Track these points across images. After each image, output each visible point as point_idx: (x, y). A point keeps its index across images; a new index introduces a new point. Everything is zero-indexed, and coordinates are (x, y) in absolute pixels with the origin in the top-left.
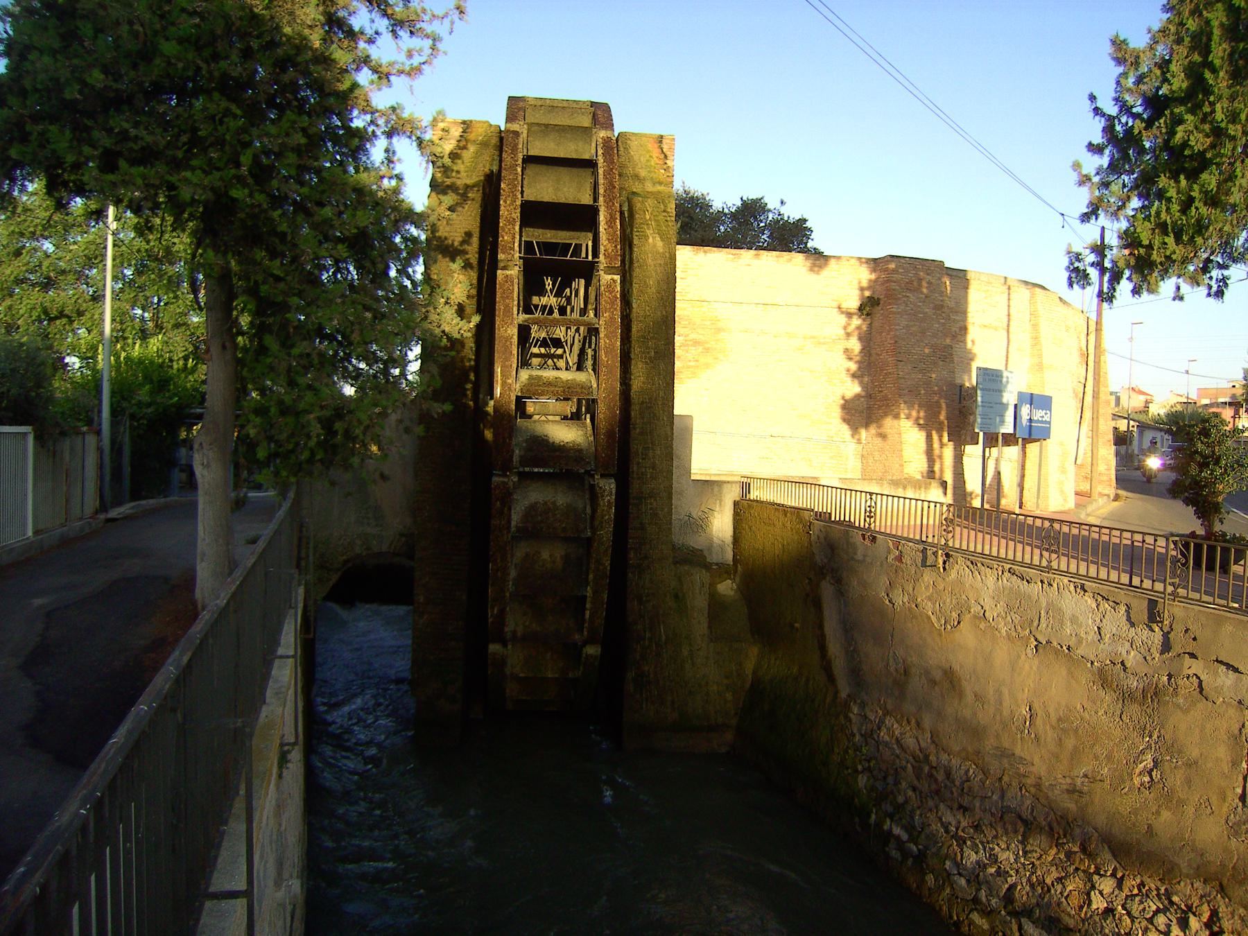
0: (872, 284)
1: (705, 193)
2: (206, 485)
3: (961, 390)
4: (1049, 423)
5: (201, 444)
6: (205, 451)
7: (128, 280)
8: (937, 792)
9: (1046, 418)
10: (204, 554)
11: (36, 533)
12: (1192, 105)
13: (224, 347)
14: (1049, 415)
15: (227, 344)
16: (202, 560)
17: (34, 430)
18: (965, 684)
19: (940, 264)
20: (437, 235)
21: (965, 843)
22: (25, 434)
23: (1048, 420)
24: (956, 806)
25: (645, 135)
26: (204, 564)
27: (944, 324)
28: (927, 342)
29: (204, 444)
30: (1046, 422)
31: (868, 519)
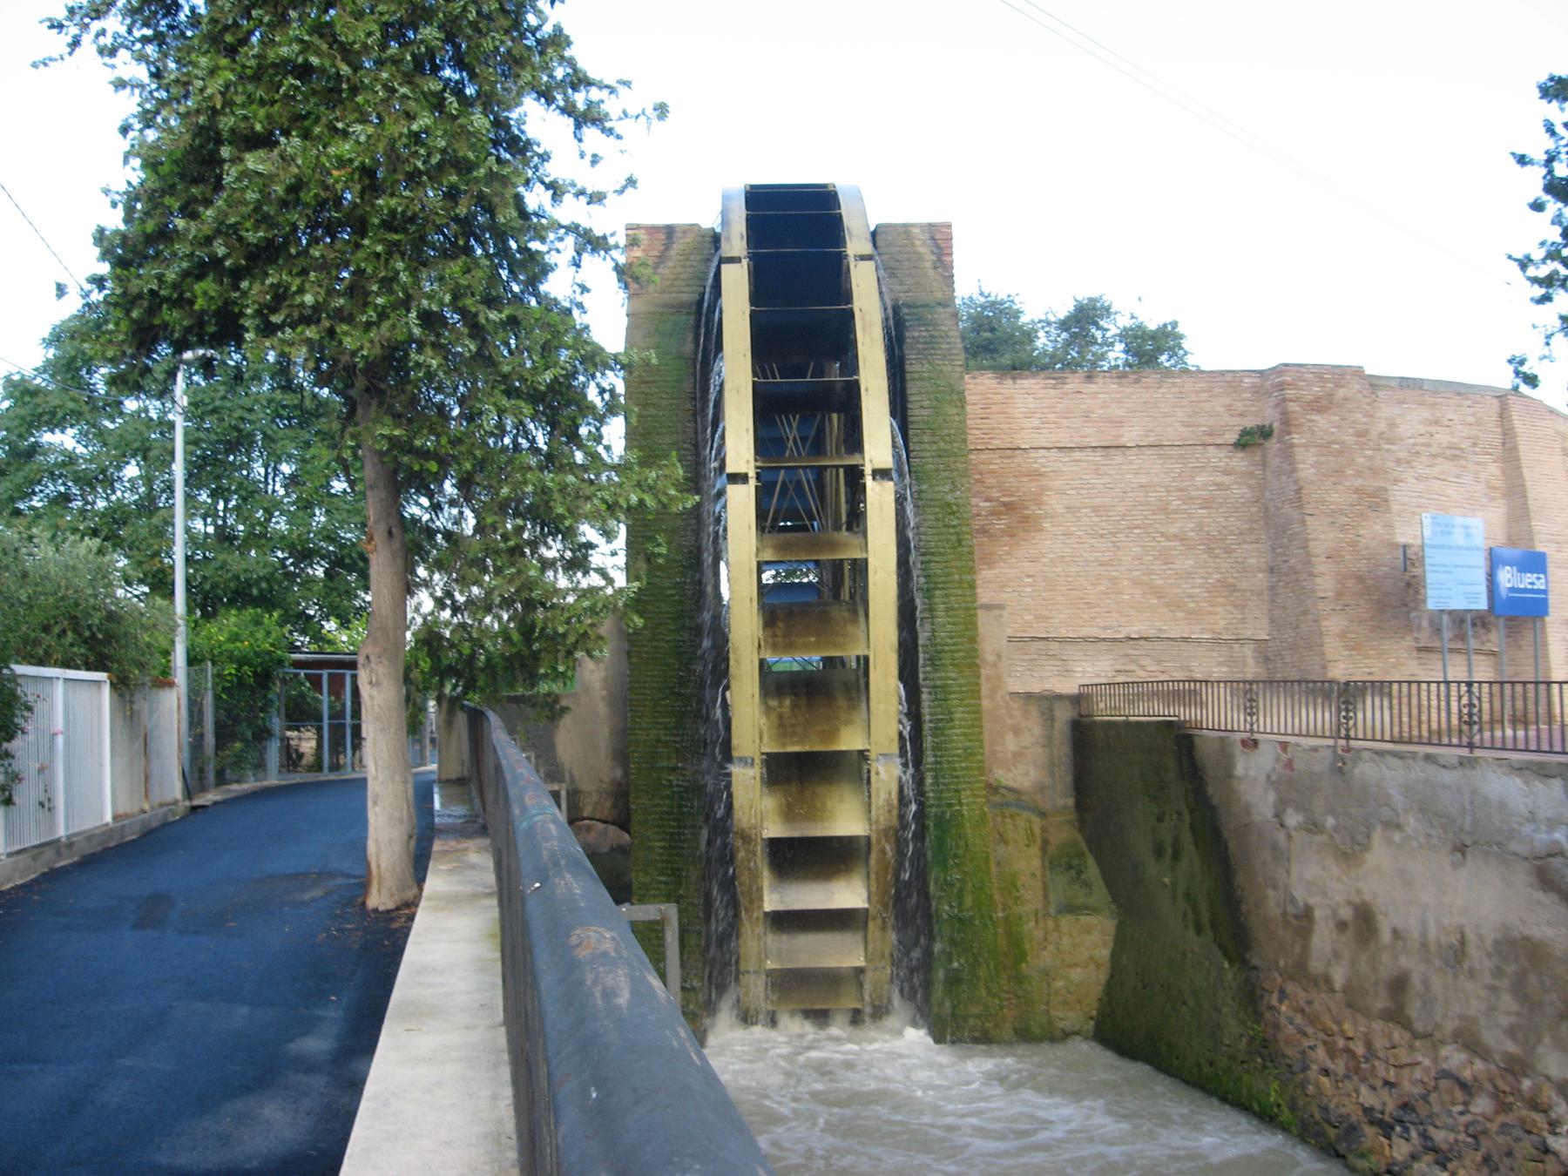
0: (121, 387)
1: (1013, 294)
2: (376, 707)
3: (1405, 552)
4: (1545, 592)
5: (368, 657)
6: (372, 665)
7: (1089, 357)
8: (1357, 1070)
9: (1540, 585)
10: (377, 796)
11: (116, 818)
12: (458, 486)
13: (390, 533)
14: (1543, 581)
15: (394, 530)
16: (375, 803)
17: (109, 678)
18: (1380, 918)
19: (1357, 372)
20: (165, 306)
21: (1392, 1128)
22: (98, 683)
23: (1543, 587)
24: (1379, 1083)
25: (913, 225)
26: (377, 809)
27: (1371, 458)
28: (1347, 484)
29: (372, 658)
30: (1539, 591)
31: (1248, 718)
